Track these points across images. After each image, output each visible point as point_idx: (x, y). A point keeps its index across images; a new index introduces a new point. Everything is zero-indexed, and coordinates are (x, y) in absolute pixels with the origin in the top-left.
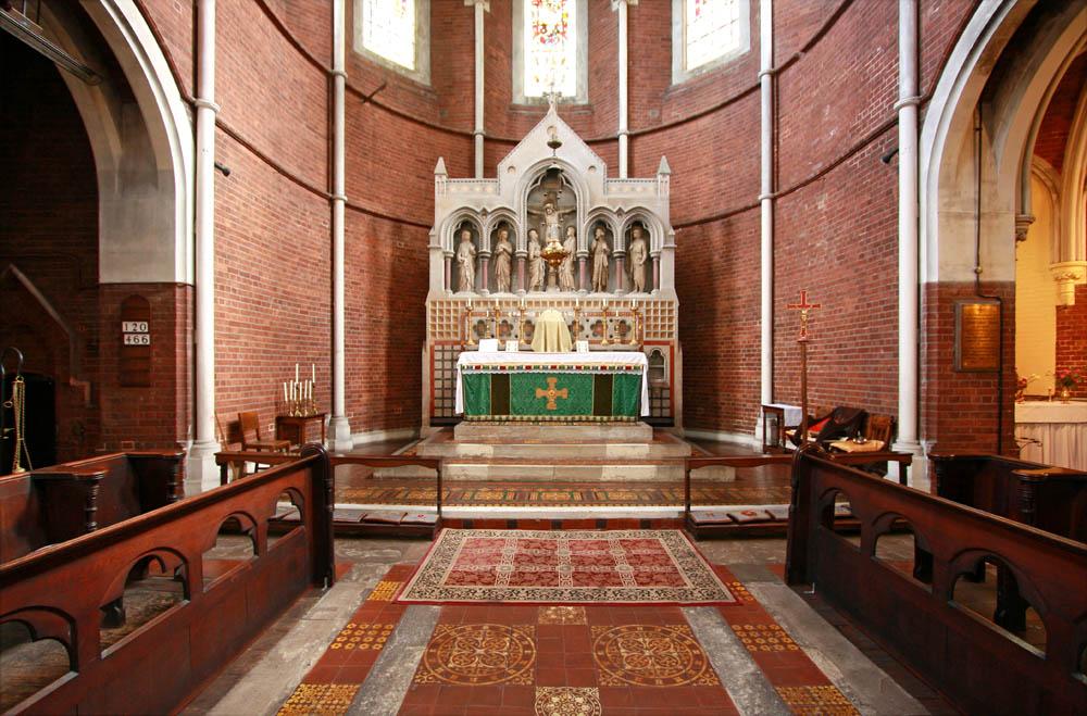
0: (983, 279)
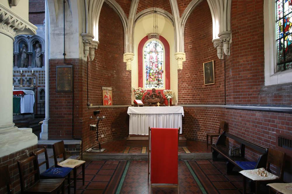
0: (67, 57)
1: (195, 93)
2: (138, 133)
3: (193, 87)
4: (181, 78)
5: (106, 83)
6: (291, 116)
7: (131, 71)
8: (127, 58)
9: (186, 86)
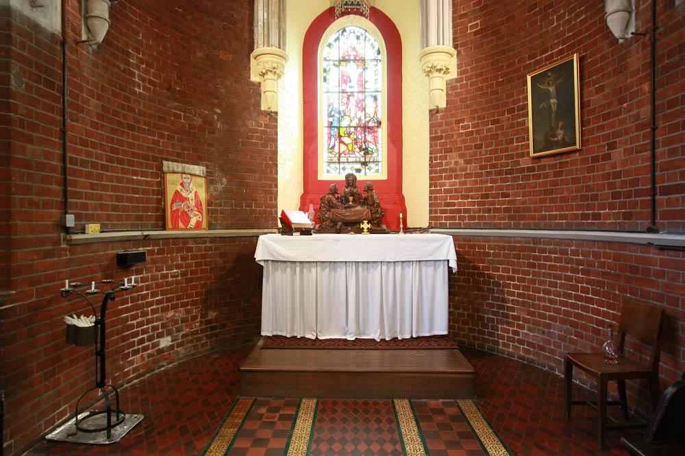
1: (491, 188)
2: (292, 330)
3: (482, 167)
4: (441, 138)
5: (184, 149)
6: (683, 256)
7: (276, 113)
8: (261, 69)
9: (456, 163)
